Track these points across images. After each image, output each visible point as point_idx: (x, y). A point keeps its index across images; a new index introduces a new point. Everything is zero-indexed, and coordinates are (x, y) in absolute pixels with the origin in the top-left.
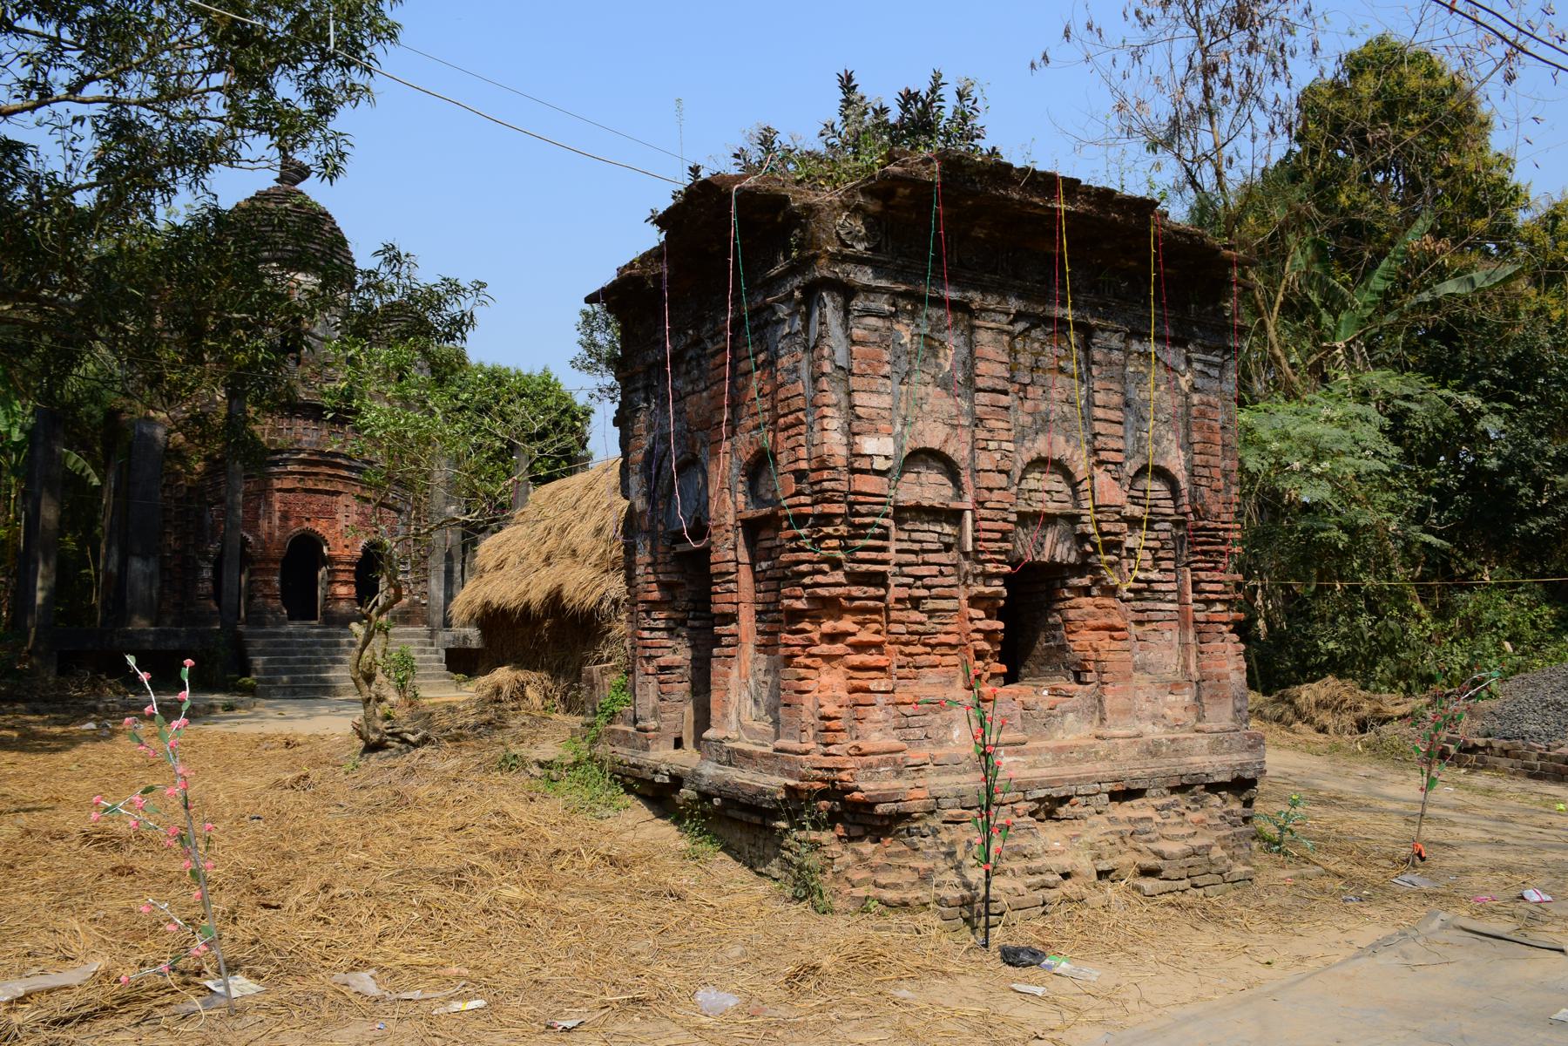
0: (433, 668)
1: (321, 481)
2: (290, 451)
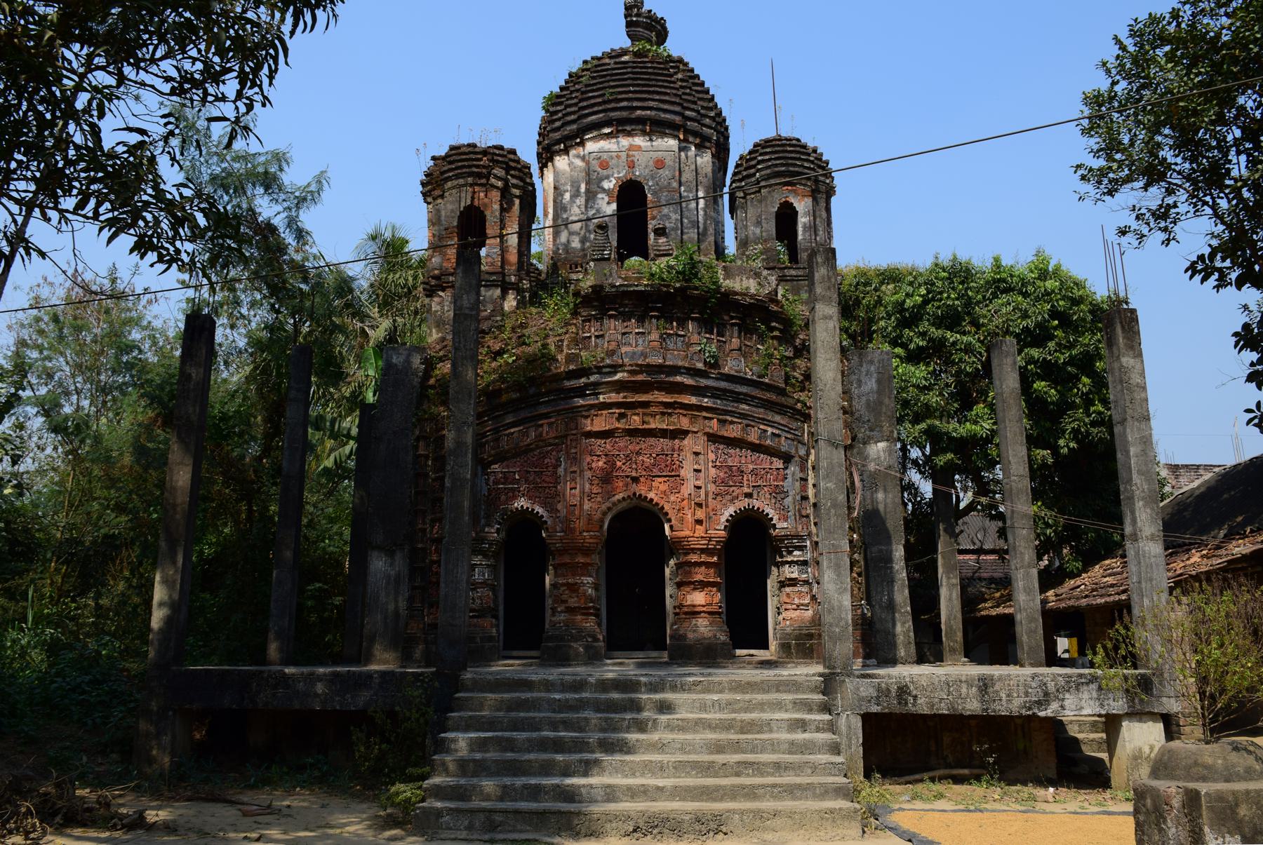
0: (815, 768)
1: (653, 415)
2: (599, 370)
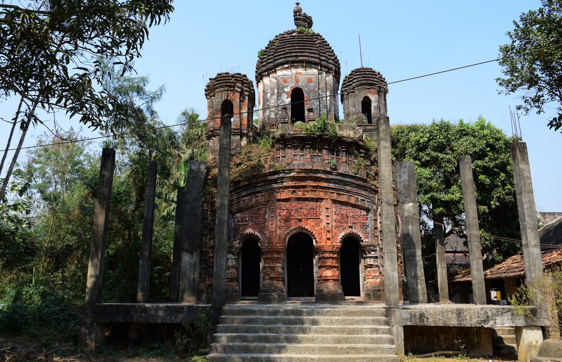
0: (382, 351)
1: (308, 192)
2: (284, 171)
